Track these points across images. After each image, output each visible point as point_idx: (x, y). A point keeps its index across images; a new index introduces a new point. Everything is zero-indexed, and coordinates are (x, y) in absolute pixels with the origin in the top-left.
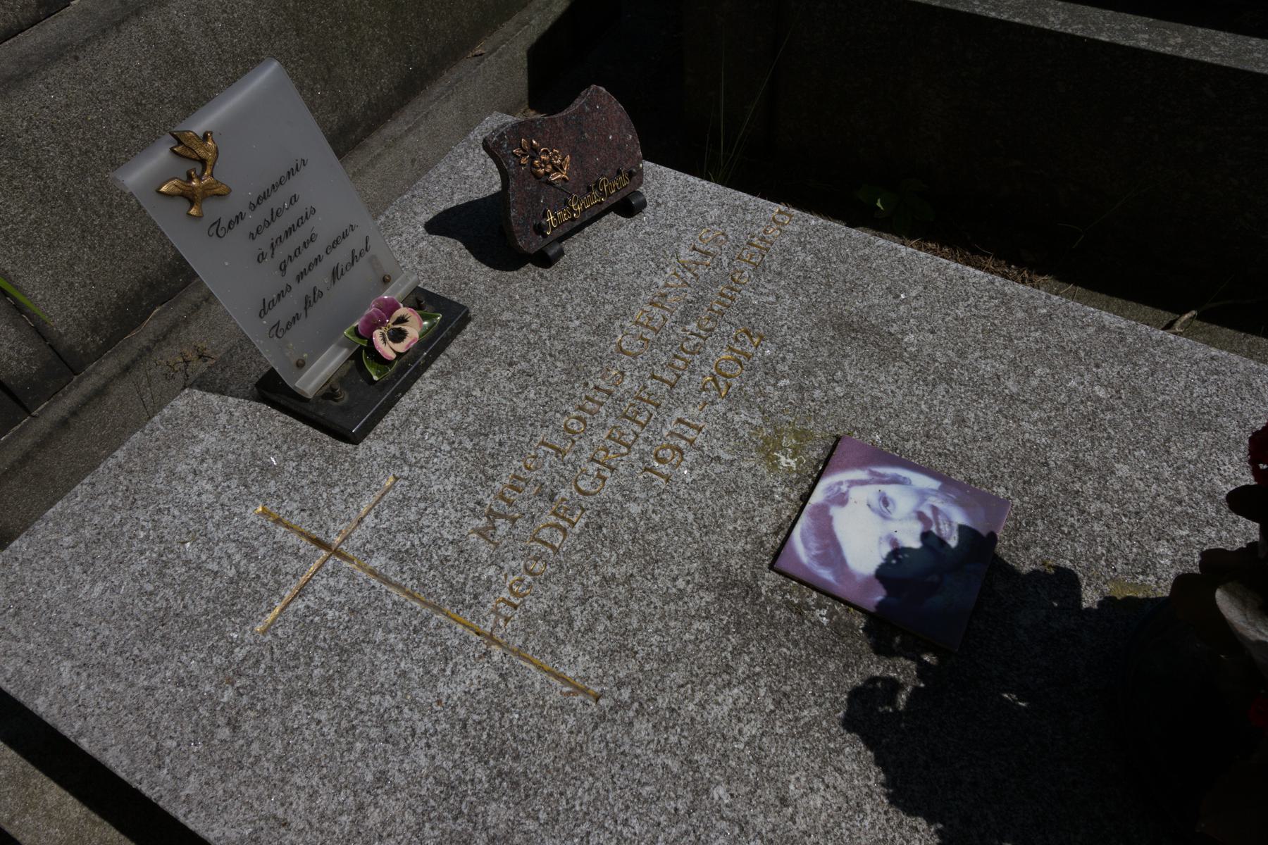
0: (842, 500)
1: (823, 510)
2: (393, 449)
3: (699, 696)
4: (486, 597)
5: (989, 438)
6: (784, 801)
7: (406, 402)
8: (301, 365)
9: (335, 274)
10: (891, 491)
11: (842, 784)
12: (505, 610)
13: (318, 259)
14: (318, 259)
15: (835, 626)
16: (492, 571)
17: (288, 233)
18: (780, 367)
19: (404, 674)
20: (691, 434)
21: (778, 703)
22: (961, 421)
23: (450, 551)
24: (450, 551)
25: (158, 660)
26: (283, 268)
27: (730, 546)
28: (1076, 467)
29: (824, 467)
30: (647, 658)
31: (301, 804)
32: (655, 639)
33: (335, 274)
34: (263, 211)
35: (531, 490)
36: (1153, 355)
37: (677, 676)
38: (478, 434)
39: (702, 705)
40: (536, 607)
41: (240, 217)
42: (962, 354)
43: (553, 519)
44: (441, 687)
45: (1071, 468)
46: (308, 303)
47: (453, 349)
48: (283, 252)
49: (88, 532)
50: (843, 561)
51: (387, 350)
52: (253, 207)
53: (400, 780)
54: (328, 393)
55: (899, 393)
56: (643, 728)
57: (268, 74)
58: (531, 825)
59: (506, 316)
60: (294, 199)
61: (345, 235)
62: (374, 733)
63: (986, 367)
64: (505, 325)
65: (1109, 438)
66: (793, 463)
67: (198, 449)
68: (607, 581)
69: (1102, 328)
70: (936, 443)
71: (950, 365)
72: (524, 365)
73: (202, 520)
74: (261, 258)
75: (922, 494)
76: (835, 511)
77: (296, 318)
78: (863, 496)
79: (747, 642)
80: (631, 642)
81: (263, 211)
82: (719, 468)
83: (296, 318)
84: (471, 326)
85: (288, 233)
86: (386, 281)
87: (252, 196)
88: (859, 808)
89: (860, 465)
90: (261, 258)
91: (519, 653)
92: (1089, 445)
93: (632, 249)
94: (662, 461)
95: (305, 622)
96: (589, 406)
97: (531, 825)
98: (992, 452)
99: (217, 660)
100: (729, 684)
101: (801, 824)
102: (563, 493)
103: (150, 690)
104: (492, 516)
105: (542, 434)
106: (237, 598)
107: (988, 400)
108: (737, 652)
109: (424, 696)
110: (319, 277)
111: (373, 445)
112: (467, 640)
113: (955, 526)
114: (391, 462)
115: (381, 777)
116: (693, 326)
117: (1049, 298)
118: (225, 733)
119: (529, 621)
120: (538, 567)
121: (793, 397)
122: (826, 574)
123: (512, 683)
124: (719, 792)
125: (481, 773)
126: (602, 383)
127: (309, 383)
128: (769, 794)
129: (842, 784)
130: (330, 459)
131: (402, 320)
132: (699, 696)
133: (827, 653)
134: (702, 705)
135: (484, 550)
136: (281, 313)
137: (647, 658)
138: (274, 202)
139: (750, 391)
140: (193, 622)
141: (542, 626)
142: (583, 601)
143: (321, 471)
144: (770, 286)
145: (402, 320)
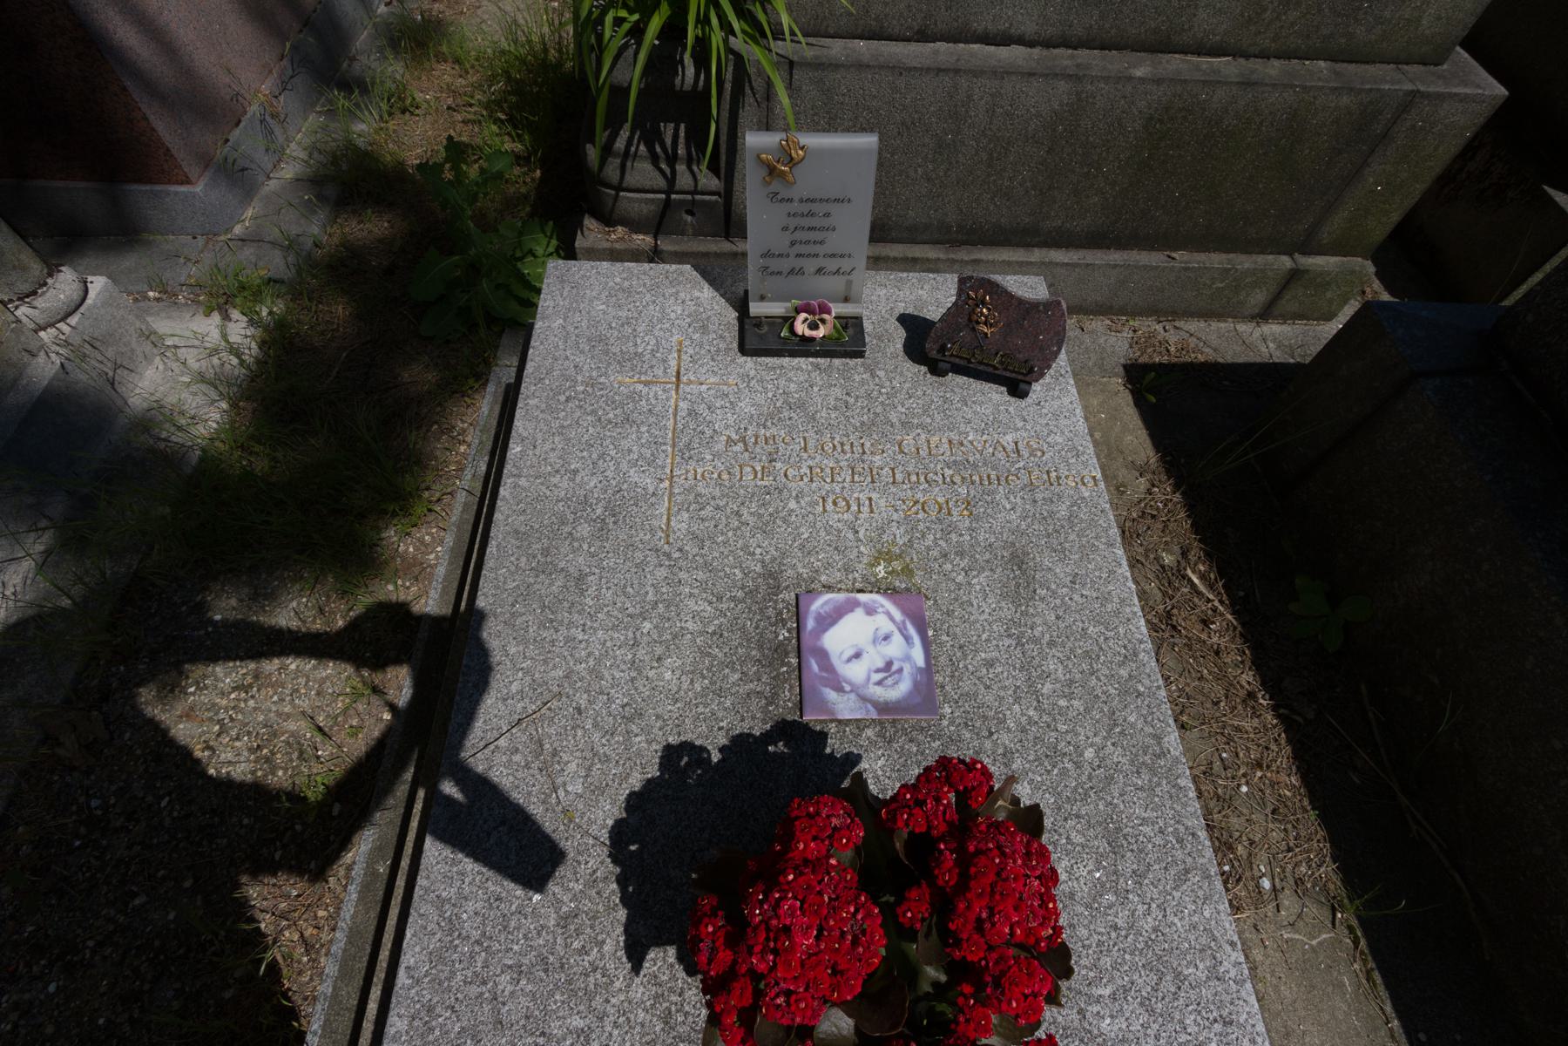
0: (870, 611)
1: (857, 604)
2: (752, 373)
3: (696, 591)
4: (693, 463)
5: (987, 687)
6: (659, 659)
7: (786, 361)
8: (762, 298)
9: (819, 271)
10: (897, 638)
11: (685, 686)
12: (691, 476)
13: (816, 255)
14: (816, 255)
15: (781, 644)
16: (709, 457)
17: (810, 229)
18: (953, 536)
19: (630, 451)
20: (866, 509)
21: (715, 633)
22: (990, 664)
23: (709, 433)
24: (709, 433)
25: (582, 352)
26: (793, 244)
27: (799, 565)
28: (1004, 755)
29: (890, 592)
30: (702, 556)
31: (548, 446)
32: (716, 554)
33: (819, 271)
34: (805, 208)
35: (770, 448)
36: (1159, 784)
37: (701, 575)
38: (789, 404)
39: (691, 595)
40: (701, 489)
41: (790, 200)
42: (1052, 644)
43: (758, 468)
44: (632, 471)
45: (1000, 751)
46: (791, 272)
47: (837, 362)
48: (799, 235)
49: (626, 284)
50: (825, 630)
51: (801, 328)
52: (801, 201)
53: (578, 479)
54: (758, 322)
55: (986, 616)
56: (662, 573)
57: (870, 141)
58: (585, 547)
59: (881, 373)
60: (827, 215)
61: (842, 256)
62: (595, 456)
63: (1051, 665)
64: (873, 376)
65: (1048, 772)
66: (882, 574)
67: (697, 294)
68: (738, 514)
69: (1158, 738)
70: (959, 654)
71: (1036, 641)
72: (852, 401)
73: (660, 321)
74: (785, 229)
75: (908, 658)
76: (859, 612)
77: (779, 273)
78: (882, 623)
79: (743, 601)
80: (708, 543)
81: (805, 208)
82: (850, 536)
83: (779, 273)
84: (859, 361)
85: (810, 229)
86: (846, 300)
87: (805, 195)
88: (677, 701)
89: (905, 612)
90: (785, 229)
91: (671, 495)
92: (1031, 758)
93: (986, 410)
94: (835, 503)
95: (634, 397)
96: (847, 448)
97: (585, 547)
98: (976, 694)
99: (594, 374)
100: (710, 603)
101: (651, 674)
102: (778, 465)
103: (567, 358)
104: (743, 440)
105: (811, 434)
106: (629, 361)
107: (1022, 676)
108: (733, 599)
109: (624, 466)
110: (810, 265)
111: (749, 363)
112: (663, 467)
113: (190, 167)
114: (746, 377)
115: (576, 472)
116: (948, 472)
117: (1159, 688)
118: (563, 398)
119: (690, 490)
120: (725, 476)
121: (935, 553)
122: (810, 624)
123: (653, 500)
124: (647, 626)
125: (599, 512)
126: (868, 445)
127: (756, 309)
128: (659, 650)
129: (685, 686)
130: (728, 350)
131: (823, 321)
132: (696, 591)
133: (761, 647)
134: (691, 595)
135: (720, 447)
136: (775, 264)
137: (702, 556)
138: (815, 207)
139: (921, 526)
140: (606, 353)
141: (691, 497)
142: (718, 508)
143: (718, 351)
144: (1018, 500)
145: (823, 321)
